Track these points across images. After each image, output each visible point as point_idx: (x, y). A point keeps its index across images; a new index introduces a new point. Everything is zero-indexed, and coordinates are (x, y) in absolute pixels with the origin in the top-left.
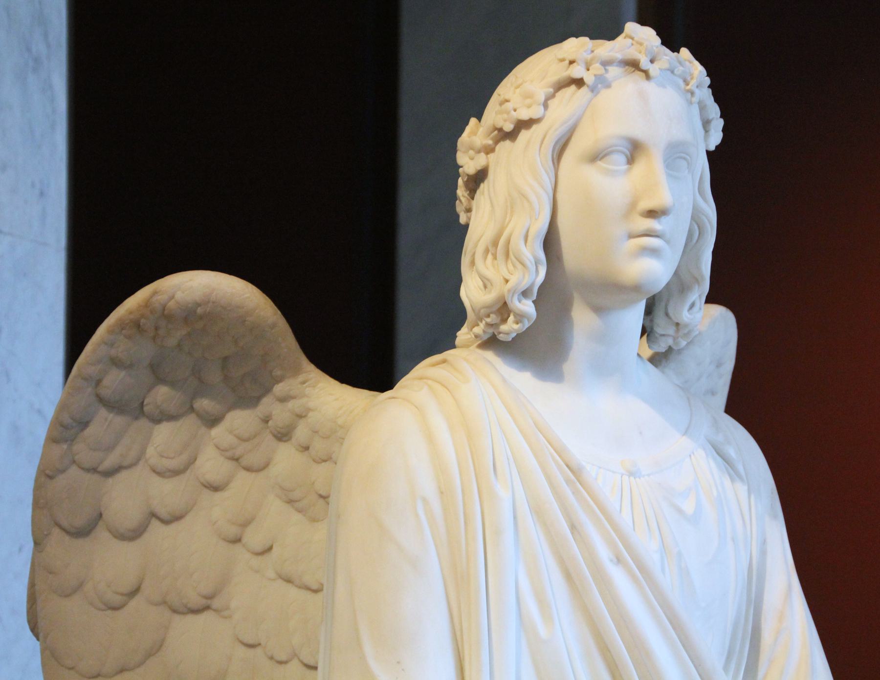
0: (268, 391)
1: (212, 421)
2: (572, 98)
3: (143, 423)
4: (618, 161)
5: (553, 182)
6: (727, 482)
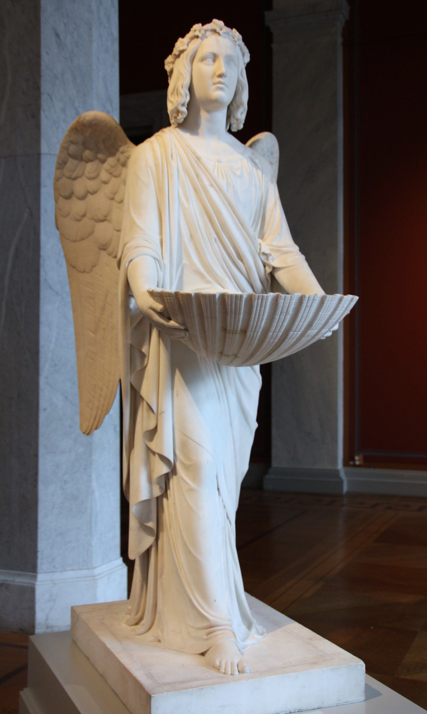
0: (117, 150)
1: (103, 162)
2: (196, 42)
3: (83, 163)
4: (210, 61)
5: (191, 68)
6: (254, 169)
